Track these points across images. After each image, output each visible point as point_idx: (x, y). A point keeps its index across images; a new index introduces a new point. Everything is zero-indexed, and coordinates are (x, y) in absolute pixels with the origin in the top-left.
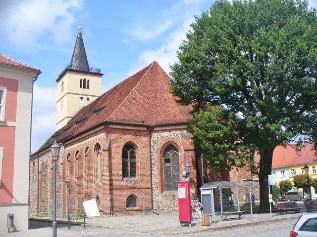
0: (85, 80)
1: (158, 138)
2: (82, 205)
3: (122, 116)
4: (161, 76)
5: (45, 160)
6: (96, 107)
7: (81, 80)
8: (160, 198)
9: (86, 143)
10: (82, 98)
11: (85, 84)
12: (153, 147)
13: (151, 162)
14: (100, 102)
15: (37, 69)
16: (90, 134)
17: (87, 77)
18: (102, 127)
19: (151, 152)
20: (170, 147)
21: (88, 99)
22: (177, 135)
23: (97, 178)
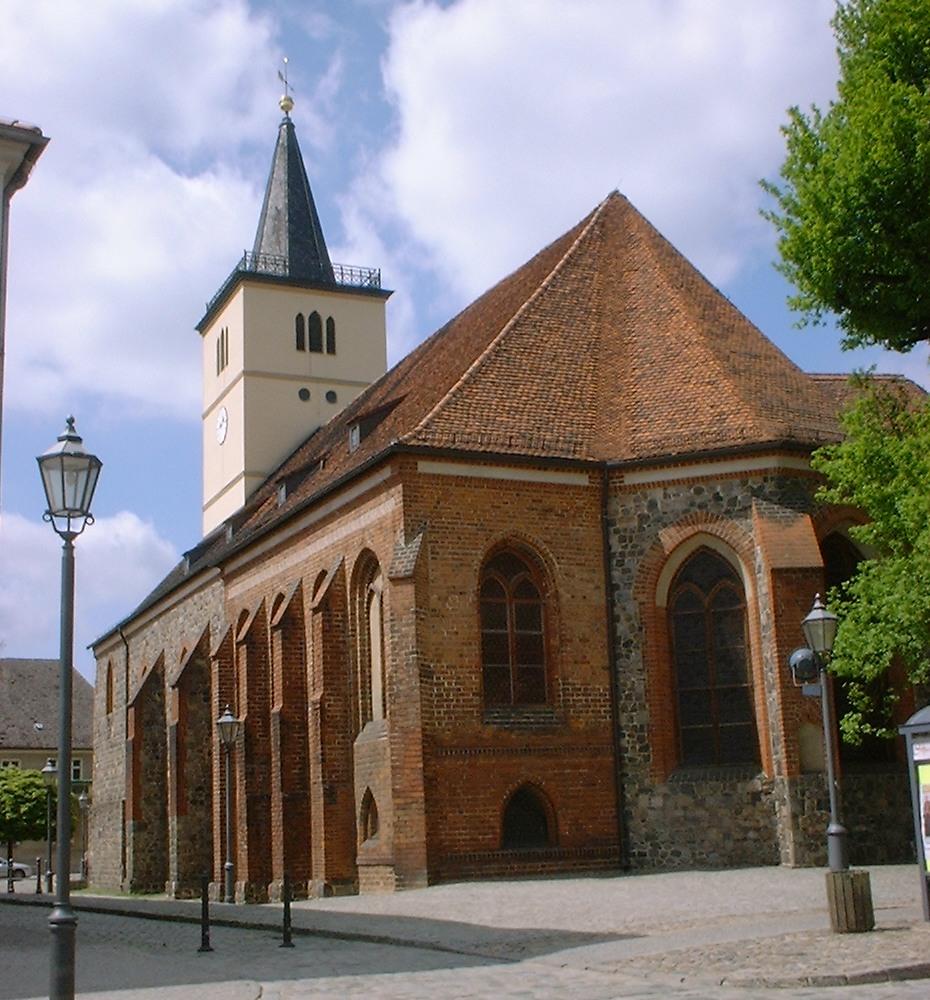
4: (644, 253)
6: (368, 418)
7: (300, 317)
10: (304, 395)
11: (315, 336)
12: (621, 563)
15: (27, 120)
18: (386, 473)
21: (331, 397)
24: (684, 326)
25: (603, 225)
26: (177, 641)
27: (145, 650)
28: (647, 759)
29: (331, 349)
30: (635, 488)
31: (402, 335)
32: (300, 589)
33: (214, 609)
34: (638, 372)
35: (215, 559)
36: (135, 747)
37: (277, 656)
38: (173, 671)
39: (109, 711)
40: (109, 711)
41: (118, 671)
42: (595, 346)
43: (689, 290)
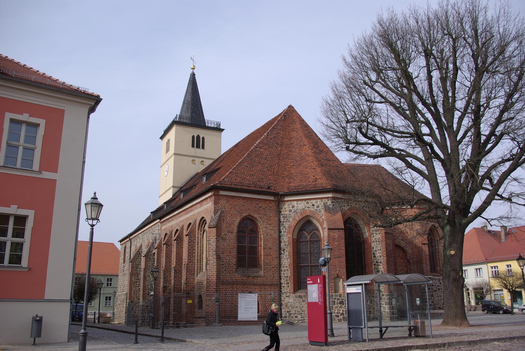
0: (198, 137)
1: (290, 211)
2: (240, 321)
3: (239, 180)
5: (139, 245)
6: (209, 172)
7: (193, 137)
8: (291, 300)
9: (188, 219)
11: (198, 143)
13: (280, 245)
14: (215, 165)
15: (96, 93)
16: (193, 206)
17: (202, 133)
19: (280, 232)
20: (306, 224)
22: (318, 207)
23: (201, 269)
24: (308, 150)
25: (285, 116)
26: (146, 242)
27: (137, 243)
28: (288, 286)
29: (203, 148)
30: (288, 201)
31: (228, 142)
32: (182, 228)
33: (159, 229)
34: (292, 164)
35: (160, 214)
36: (131, 275)
37: (174, 249)
38: (145, 250)
39: (124, 263)
40: (124, 263)
41: (128, 250)
42: (279, 155)
43: (310, 138)
